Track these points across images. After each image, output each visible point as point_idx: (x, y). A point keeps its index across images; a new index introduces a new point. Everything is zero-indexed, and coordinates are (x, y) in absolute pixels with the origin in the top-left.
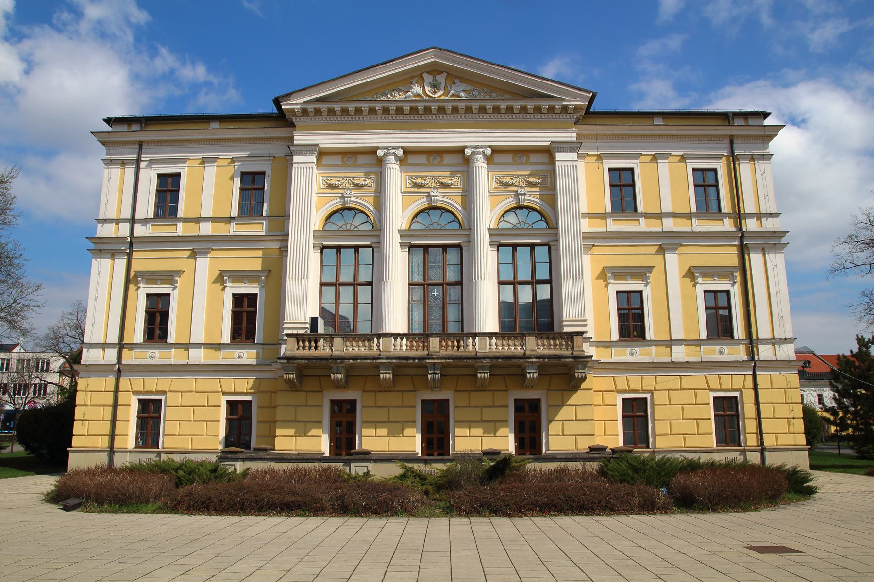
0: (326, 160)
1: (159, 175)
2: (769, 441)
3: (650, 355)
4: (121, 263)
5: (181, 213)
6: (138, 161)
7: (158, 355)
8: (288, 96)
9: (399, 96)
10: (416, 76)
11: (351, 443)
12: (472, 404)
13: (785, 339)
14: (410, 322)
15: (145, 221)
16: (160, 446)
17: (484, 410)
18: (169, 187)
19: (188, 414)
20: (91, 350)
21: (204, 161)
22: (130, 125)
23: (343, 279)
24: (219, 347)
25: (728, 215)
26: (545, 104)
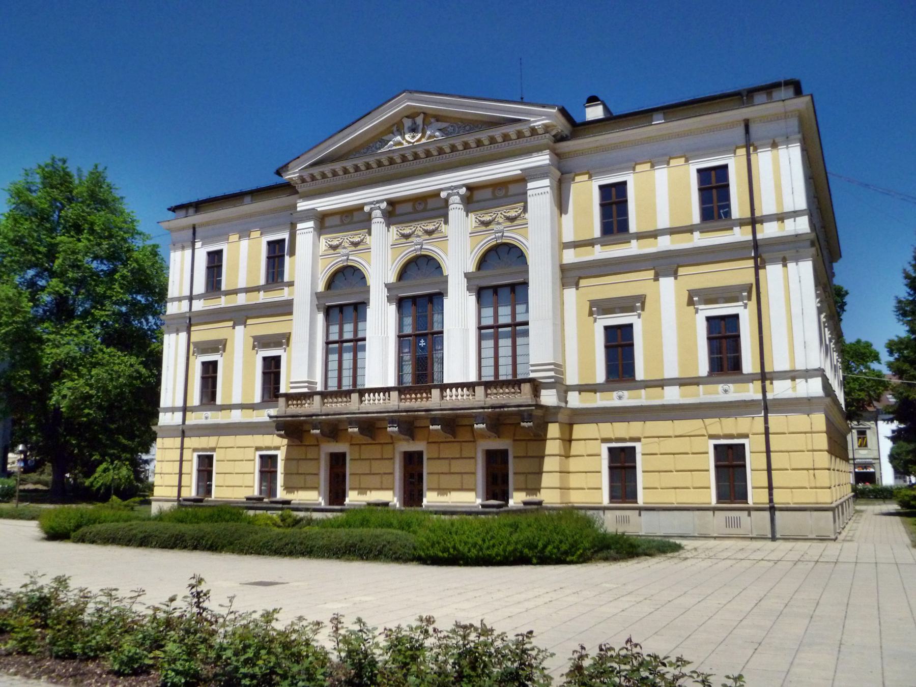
4: (183, 335)
5: (633, 227)
10: (396, 127)
15: (199, 297)
17: (453, 461)
23: (502, 321)
24: (696, 381)
26: (511, 130)
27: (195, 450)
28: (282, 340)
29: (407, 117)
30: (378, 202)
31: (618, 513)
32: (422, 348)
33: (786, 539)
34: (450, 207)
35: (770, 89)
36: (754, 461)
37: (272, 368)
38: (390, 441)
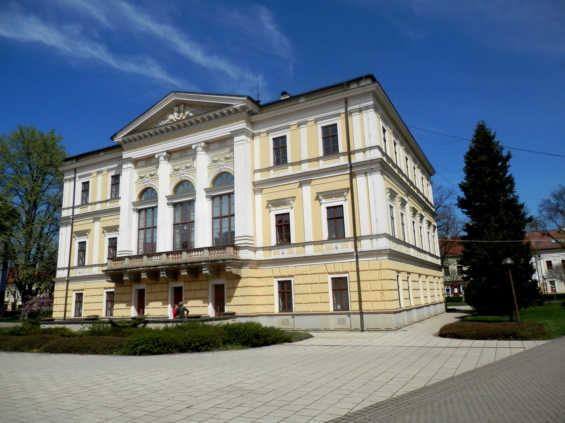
0: (140, 164)
1: (274, 139)
2: (365, 307)
3: (293, 253)
4: (69, 228)
5: (289, 161)
6: (75, 178)
7: (340, 246)
8: (115, 135)
9: (164, 123)
10: (169, 110)
11: (223, 310)
12: (191, 289)
13: (378, 235)
14: (174, 245)
15: (78, 207)
16: (294, 311)
17: (197, 292)
18: (280, 146)
19: (308, 289)
20: (379, 239)
21: (299, 125)
22: (358, 83)
23: (224, 214)
24: (322, 242)
25: (343, 154)
27: (74, 290)
28: (115, 229)
29: (176, 106)
30: (162, 152)
31: (283, 317)
32: (185, 230)
33: (369, 330)
34: (198, 153)
35: (358, 80)
36: (352, 287)
37: (113, 244)
38: (206, 279)
